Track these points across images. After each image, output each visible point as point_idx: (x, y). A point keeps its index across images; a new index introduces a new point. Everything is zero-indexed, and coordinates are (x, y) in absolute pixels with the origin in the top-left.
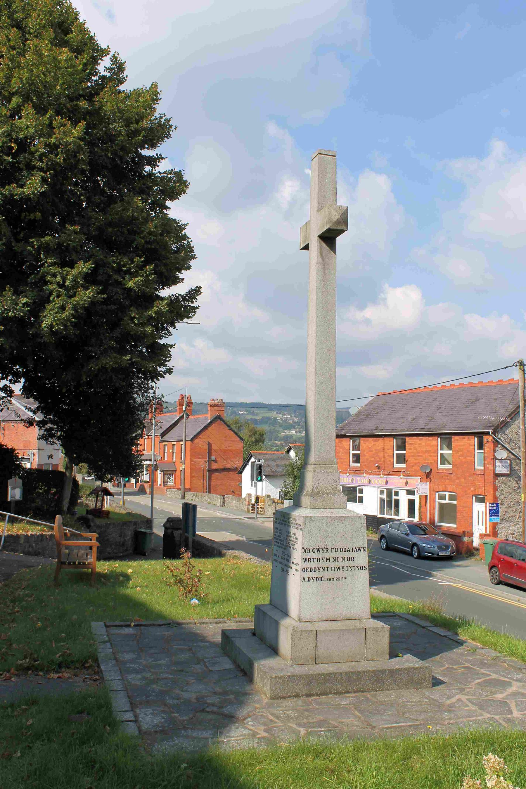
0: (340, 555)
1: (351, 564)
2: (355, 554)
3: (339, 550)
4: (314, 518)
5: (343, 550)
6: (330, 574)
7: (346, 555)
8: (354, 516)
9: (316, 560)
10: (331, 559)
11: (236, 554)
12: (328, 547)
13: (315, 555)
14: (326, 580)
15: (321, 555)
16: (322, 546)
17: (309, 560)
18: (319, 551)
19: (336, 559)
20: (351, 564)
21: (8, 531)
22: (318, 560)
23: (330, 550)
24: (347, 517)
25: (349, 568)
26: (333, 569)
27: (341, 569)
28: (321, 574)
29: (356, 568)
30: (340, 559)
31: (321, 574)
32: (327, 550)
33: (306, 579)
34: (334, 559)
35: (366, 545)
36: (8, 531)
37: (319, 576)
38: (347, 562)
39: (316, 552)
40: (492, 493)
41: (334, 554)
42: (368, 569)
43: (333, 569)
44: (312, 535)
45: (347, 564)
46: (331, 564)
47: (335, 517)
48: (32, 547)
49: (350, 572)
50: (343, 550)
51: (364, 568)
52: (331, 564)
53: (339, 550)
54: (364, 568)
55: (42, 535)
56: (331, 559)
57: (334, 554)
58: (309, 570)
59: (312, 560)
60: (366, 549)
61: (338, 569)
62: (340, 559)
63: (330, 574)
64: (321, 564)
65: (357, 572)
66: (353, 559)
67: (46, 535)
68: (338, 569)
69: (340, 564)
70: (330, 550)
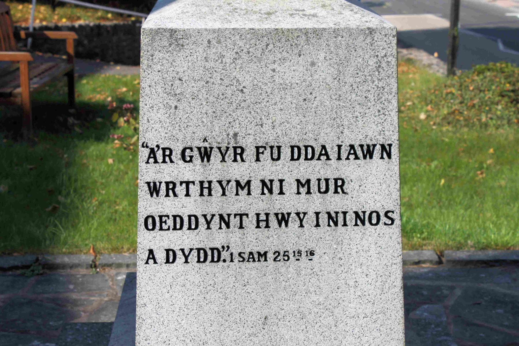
0: (288, 171)
1: (334, 202)
2: (350, 169)
3: (286, 153)
4: (186, 34)
5: (298, 153)
6: (252, 239)
7: (313, 170)
8: (349, 30)
9: (194, 189)
10: (256, 187)
11: (412, 56)
12: (242, 142)
13: (193, 171)
14: (236, 258)
15: (216, 169)
16: (218, 136)
17: (171, 187)
18: (205, 154)
19: (344, 155)
20: (334, 202)
21: (41, 20)
22: (206, 188)
23: (250, 154)
24: (318, 33)
25: (324, 219)
26: (262, 221)
27: (293, 223)
28: (217, 238)
29: (351, 217)
30: (290, 187)
31: (217, 238)
32: (239, 153)
33: (160, 256)
34: (267, 186)
35: (392, 137)
36: (44, 19)
37: (208, 245)
38: (316, 196)
39: (197, 160)
40: (290, 219)
41: (268, 169)
42: (397, 222)
43: (262, 221)
44: (179, 97)
45: (315, 203)
46: (255, 203)
47: (269, 33)
48: (83, 45)
49: (325, 230)
50: (298, 153)
51: (383, 219)
52: (255, 203)
53: (286, 153)
54: (383, 219)
55: (98, 27)
56: (256, 187)
57: (268, 169)
58: (170, 222)
59: (181, 190)
60: (395, 151)
61: (283, 219)
62: (290, 187)
63: (252, 239)
64: (216, 204)
65: (353, 234)
66: (340, 186)
67: (105, 27)
68: (283, 219)
69: (290, 202)
70: (250, 154)
